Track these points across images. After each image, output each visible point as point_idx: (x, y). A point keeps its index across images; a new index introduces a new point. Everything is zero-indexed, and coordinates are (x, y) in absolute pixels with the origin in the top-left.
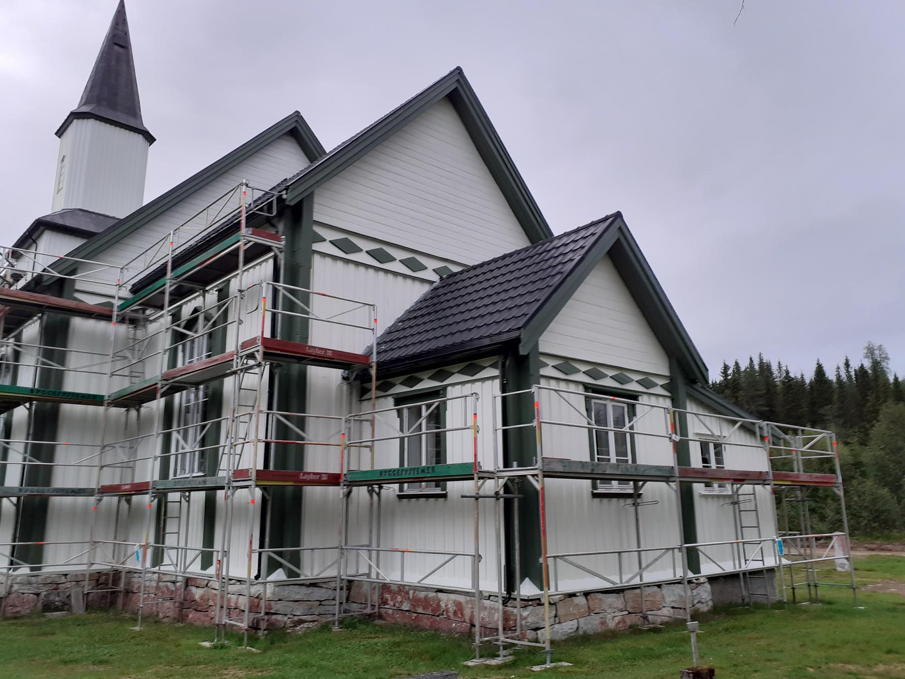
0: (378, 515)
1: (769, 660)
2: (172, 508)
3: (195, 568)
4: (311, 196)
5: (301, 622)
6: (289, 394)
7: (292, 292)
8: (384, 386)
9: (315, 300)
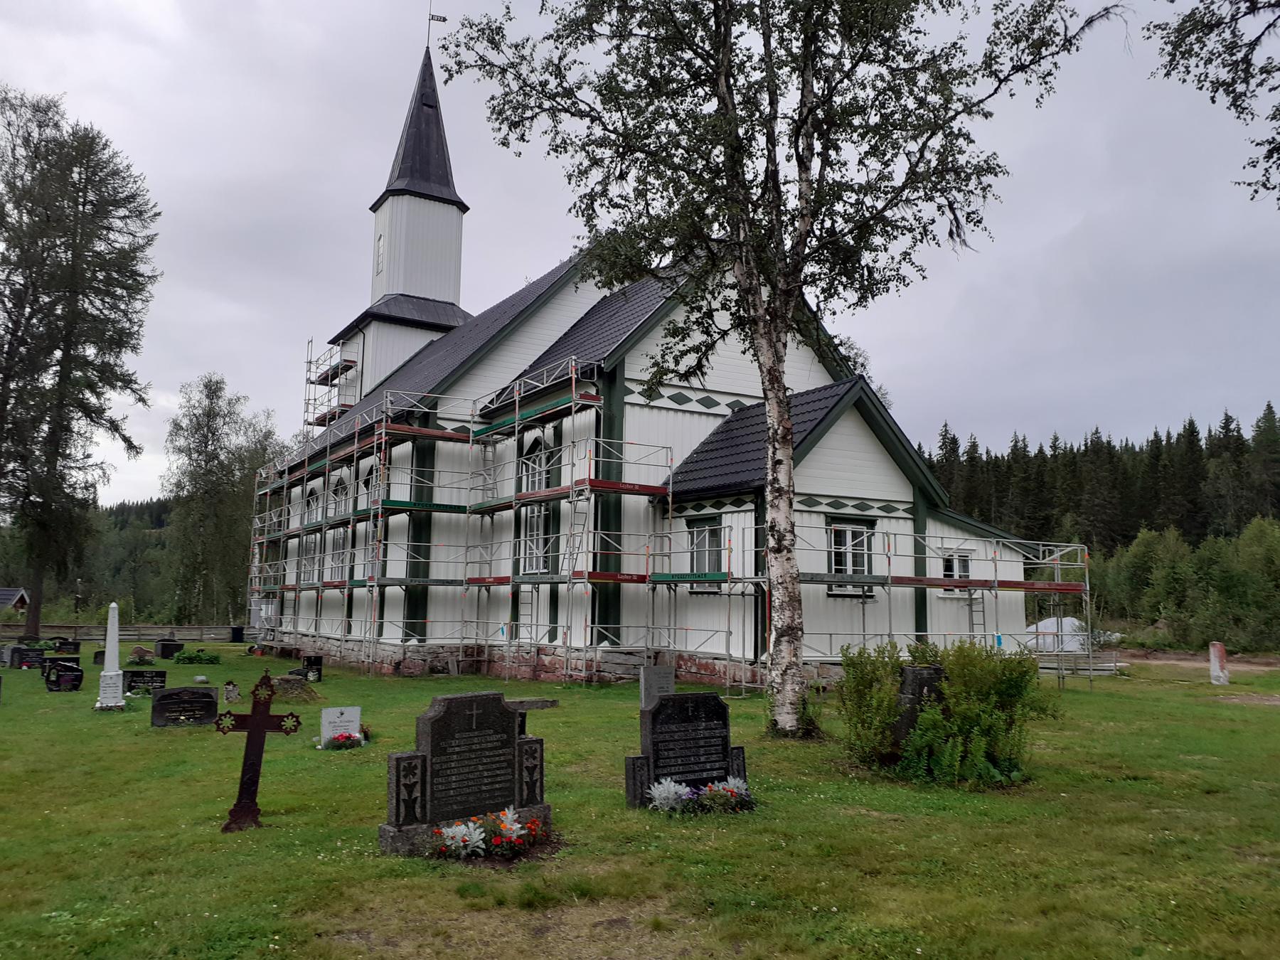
0: (675, 606)
1: (1135, 778)
2: (523, 597)
3: (545, 641)
4: (624, 359)
5: (621, 678)
6: (609, 517)
7: (610, 444)
8: (680, 509)
9: (627, 448)
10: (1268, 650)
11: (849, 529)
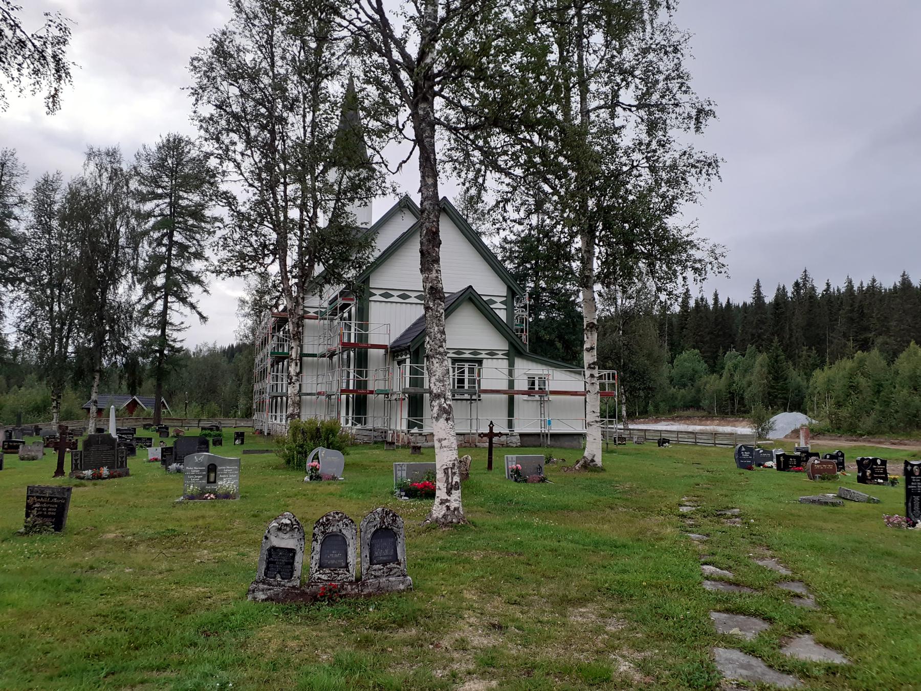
10: (883, 433)
11: (467, 365)
